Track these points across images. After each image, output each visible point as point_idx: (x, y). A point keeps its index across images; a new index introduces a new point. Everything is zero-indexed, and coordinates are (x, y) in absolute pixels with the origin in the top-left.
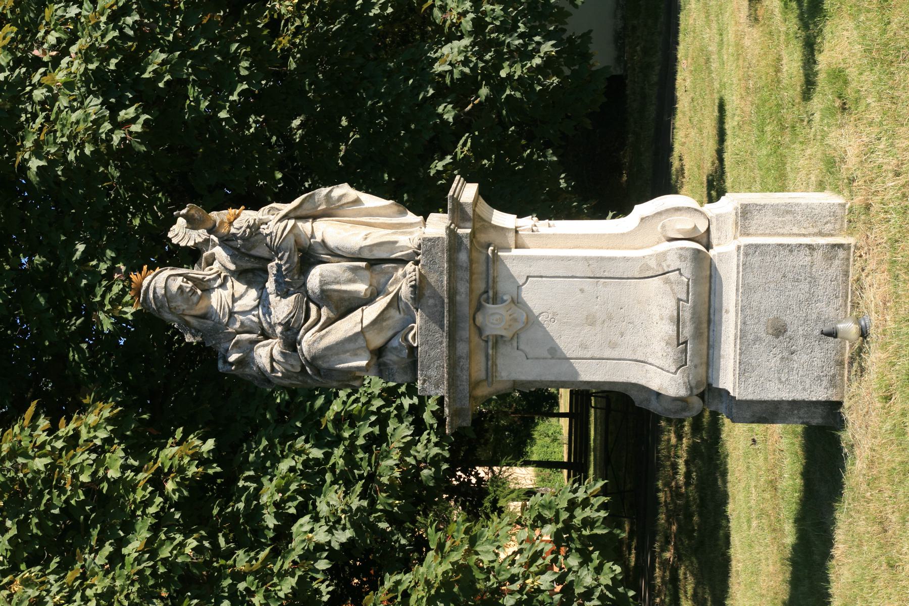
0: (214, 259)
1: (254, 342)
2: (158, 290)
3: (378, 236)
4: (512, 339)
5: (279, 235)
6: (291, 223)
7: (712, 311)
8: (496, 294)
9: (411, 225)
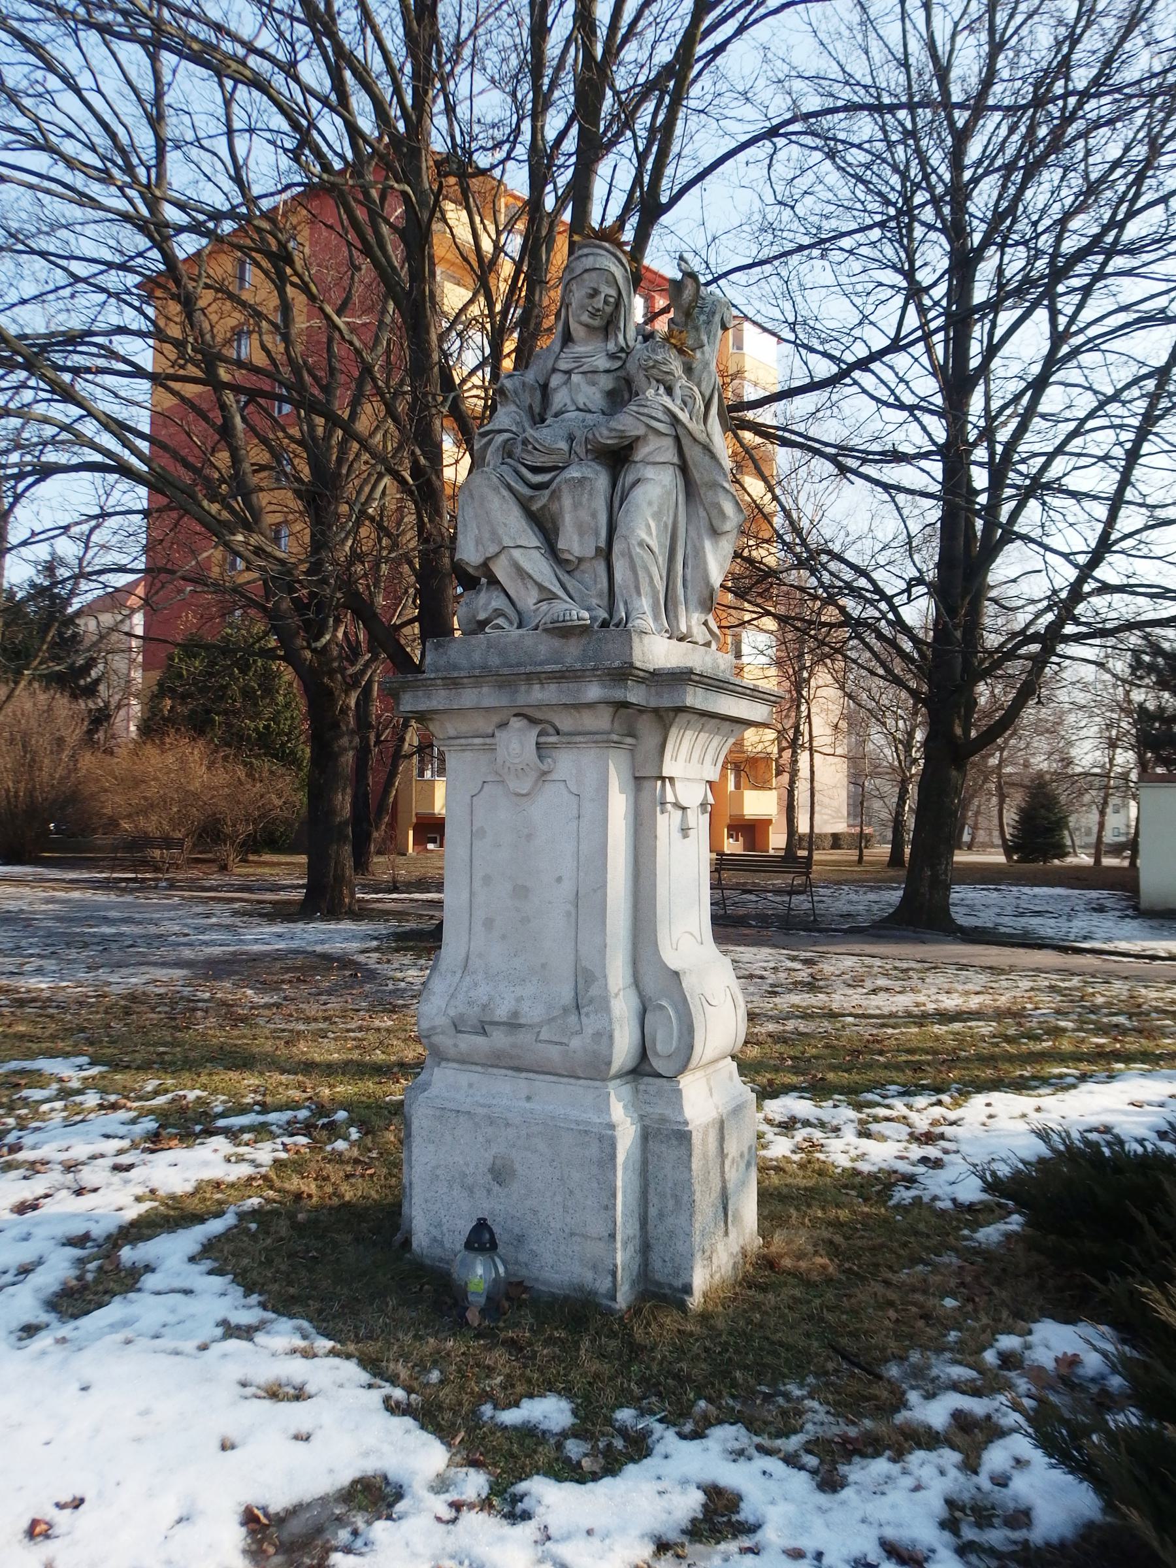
2: (591, 258)
5: (642, 410)
7: (531, 1075)
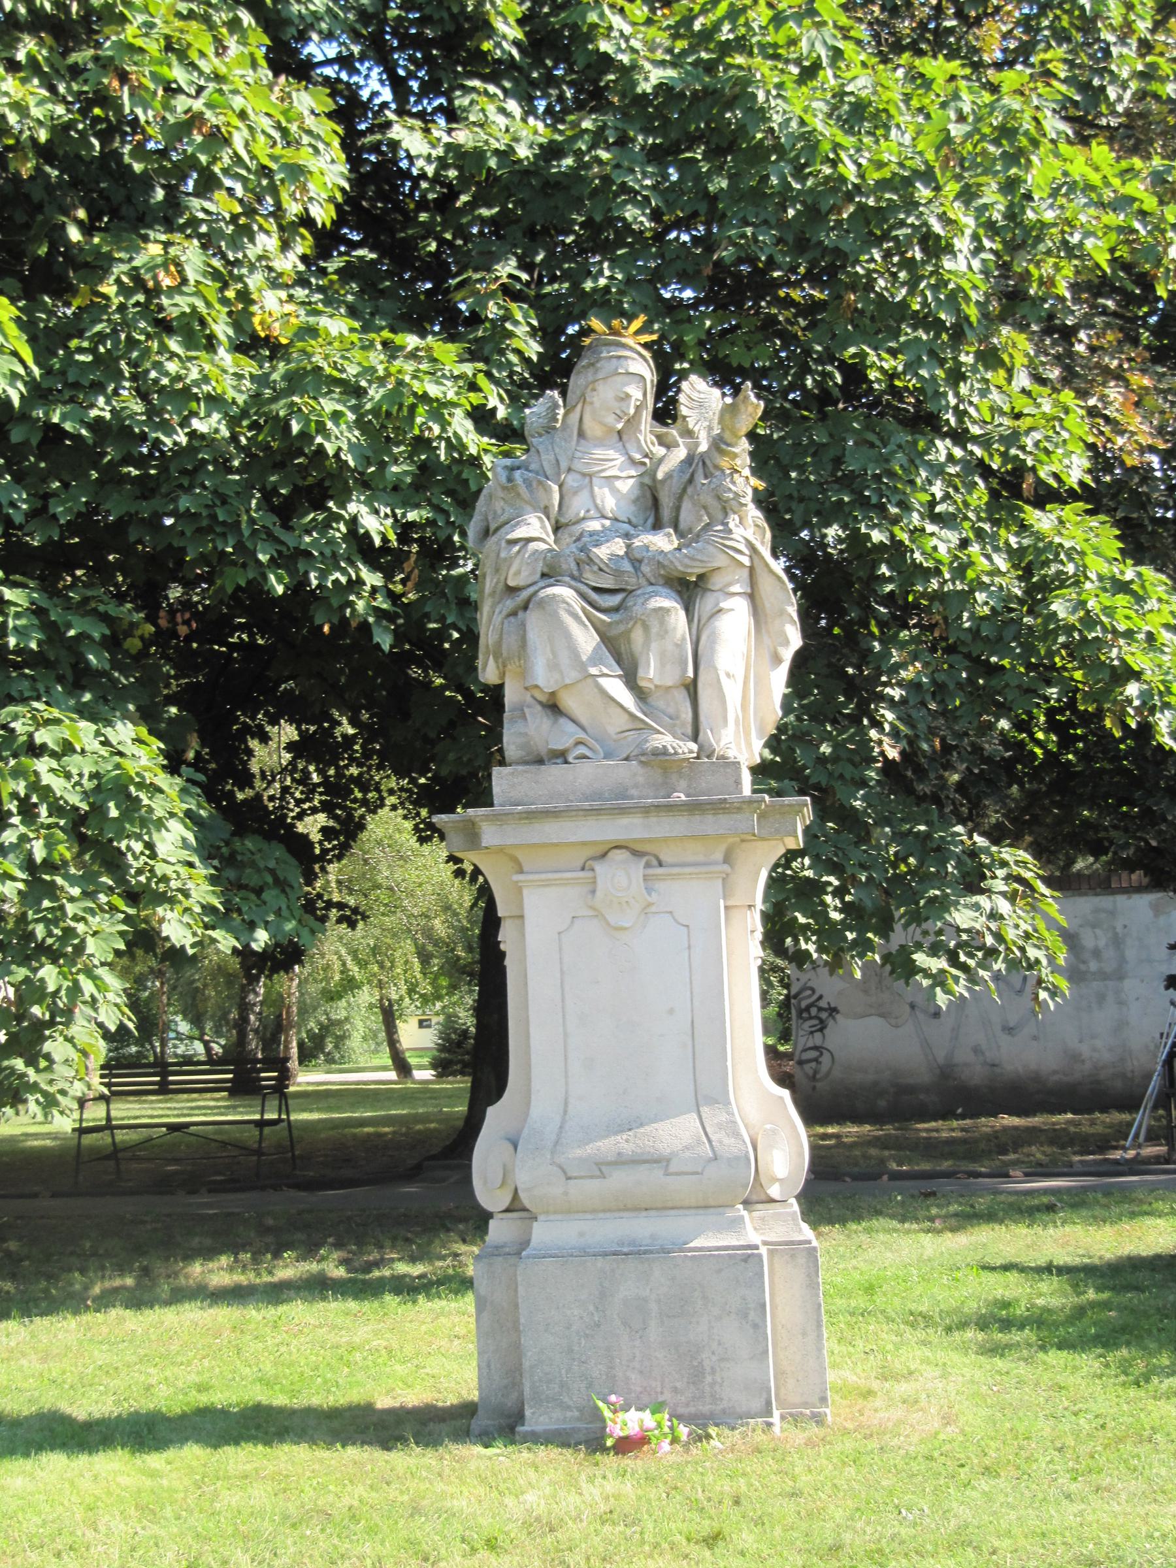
0: (668, 447)
1: (546, 511)
3: (733, 691)
4: (592, 908)
6: (746, 561)
8: (658, 878)
9: (749, 745)
